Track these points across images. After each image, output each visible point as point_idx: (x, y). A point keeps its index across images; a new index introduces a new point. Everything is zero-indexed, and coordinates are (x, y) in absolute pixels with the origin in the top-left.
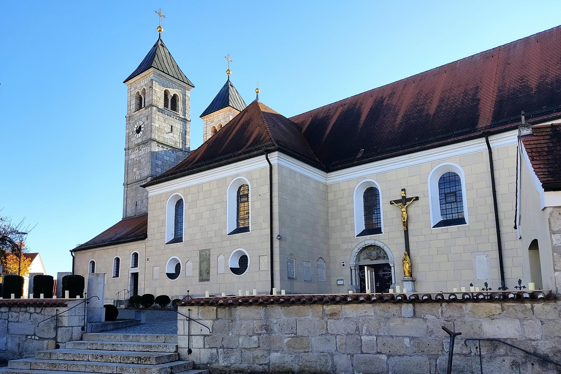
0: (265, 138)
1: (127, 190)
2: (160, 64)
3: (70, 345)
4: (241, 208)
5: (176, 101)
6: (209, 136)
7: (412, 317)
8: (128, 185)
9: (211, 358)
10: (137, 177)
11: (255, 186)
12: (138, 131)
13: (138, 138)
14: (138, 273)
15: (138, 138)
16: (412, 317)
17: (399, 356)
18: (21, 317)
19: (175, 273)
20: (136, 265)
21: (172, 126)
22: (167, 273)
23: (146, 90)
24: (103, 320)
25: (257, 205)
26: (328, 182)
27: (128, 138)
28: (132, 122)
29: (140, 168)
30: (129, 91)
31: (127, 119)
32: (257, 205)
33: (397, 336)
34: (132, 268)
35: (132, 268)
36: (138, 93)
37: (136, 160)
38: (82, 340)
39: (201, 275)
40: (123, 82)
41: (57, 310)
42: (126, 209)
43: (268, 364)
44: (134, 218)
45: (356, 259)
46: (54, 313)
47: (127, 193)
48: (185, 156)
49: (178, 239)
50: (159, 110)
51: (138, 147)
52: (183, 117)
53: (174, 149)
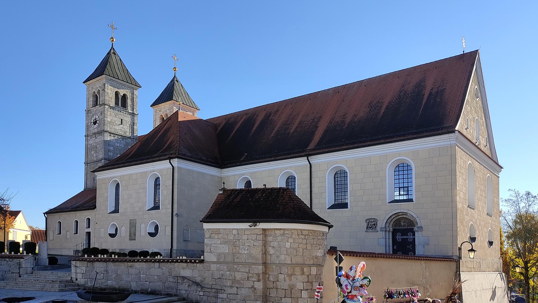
0: (175, 145)
2: (111, 71)
3: (26, 276)
6: (158, 123)
7: (158, 268)
8: (87, 164)
9: (85, 283)
10: (94, 158)
12: (95, 123)
13: (94, 128)
15: (94, 128)
16: (158, 268)
17: (153, 282)
18: (2, 262)
19: (115, 233)
20: (89, 227)
21: (122, 120)
24: (47, 264)
25: (165, 192)
26: (222, 175)
28: (90, 115)
29: (96, 152)
30: (88, 90)
32: (165, 192)
33: (153, 275)
38: (32, 274)
39: (130, 236)
41: (19, 260)
43: (107, 285)
44: (92, 189)
46: (18, 262)
48: (133, 142)
49: (116, 211)
50: (111, 107)
52: (131, 112)
53: (124, 137)
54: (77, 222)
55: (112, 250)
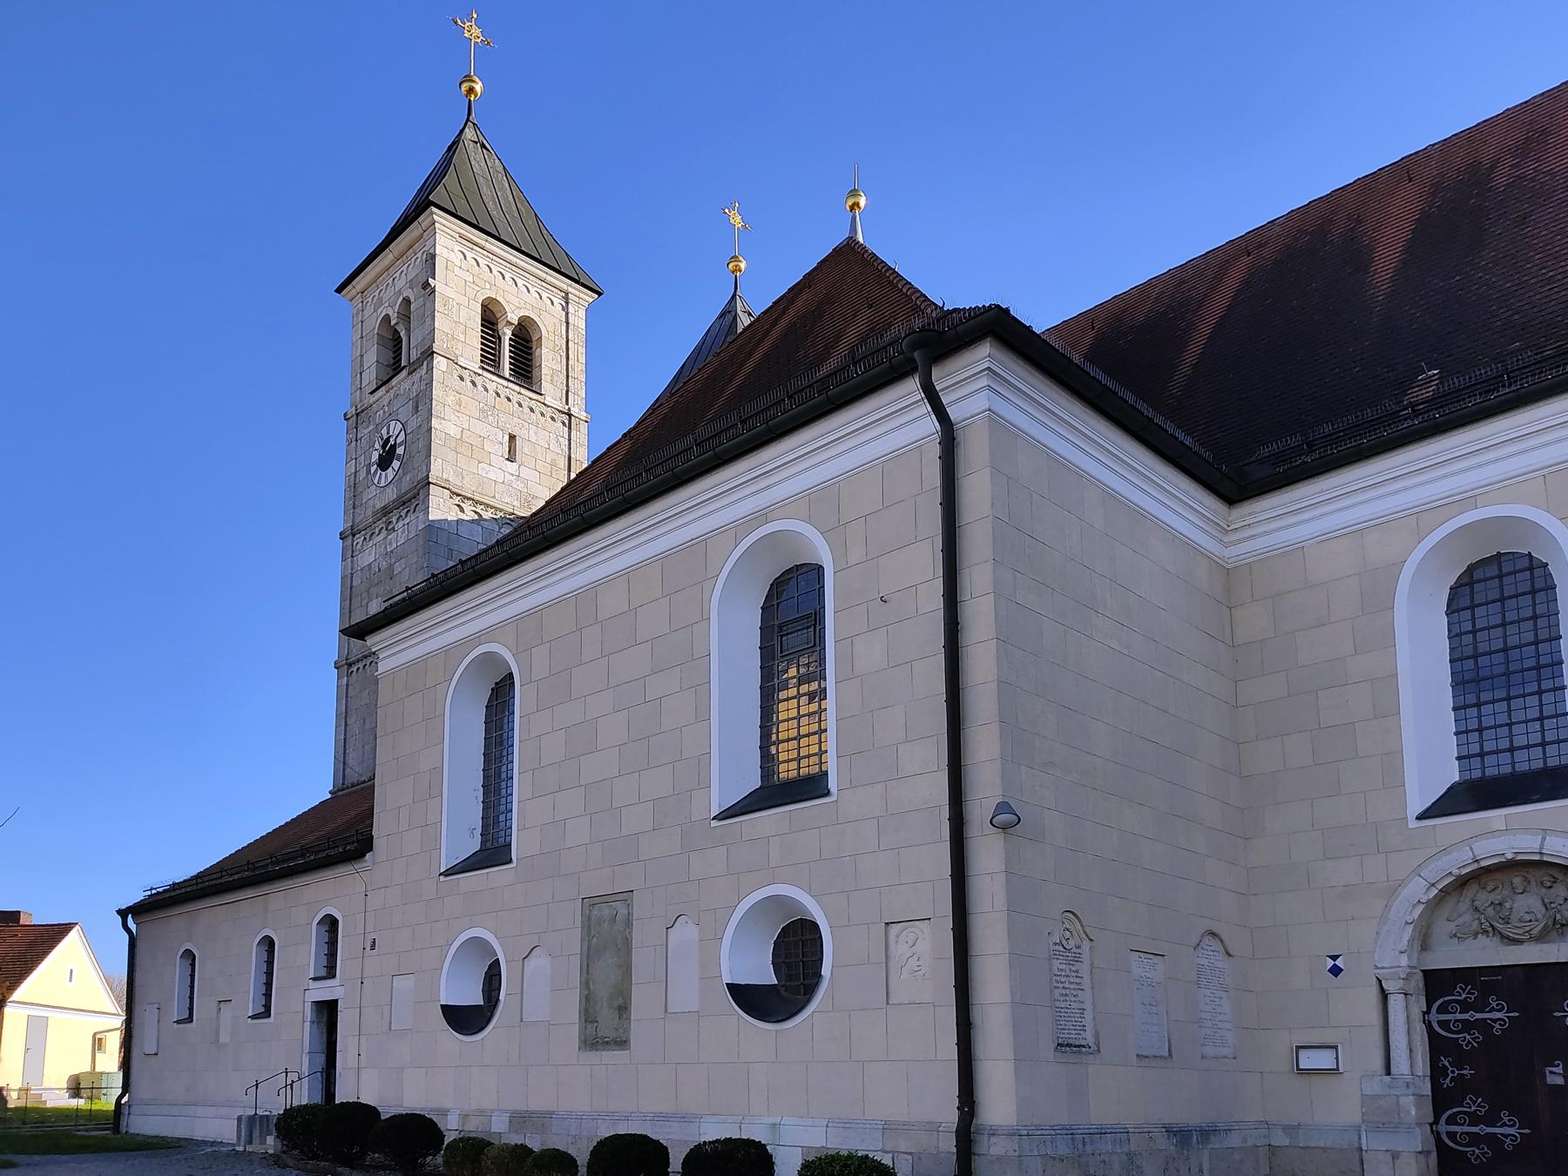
1: (347, 685)
4: (782, 726)
5: (531, 348)
8: (350, 665)
11: (855, 556)
14: (337, 1000)
15: (385, 486)
20: (331, 972)
21: (512, 438)
22: (731, 987)
23: (412, 300)
27: (354, 490)
28: (366, 431)
31: (351, 421)
34: (314, 979)
35: (314, 979)
36: (387, 318)
37: (379, 570)
39: (588, 1016)
40: (336, 291)
42: (345, 753)
45: (1411, 941)
47: (347, 697)
49: (493, 852)
51: (384, 519)
54: (269, 944)
55: (464, 1117)
